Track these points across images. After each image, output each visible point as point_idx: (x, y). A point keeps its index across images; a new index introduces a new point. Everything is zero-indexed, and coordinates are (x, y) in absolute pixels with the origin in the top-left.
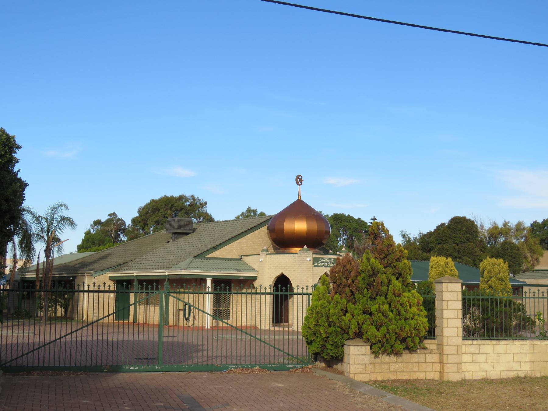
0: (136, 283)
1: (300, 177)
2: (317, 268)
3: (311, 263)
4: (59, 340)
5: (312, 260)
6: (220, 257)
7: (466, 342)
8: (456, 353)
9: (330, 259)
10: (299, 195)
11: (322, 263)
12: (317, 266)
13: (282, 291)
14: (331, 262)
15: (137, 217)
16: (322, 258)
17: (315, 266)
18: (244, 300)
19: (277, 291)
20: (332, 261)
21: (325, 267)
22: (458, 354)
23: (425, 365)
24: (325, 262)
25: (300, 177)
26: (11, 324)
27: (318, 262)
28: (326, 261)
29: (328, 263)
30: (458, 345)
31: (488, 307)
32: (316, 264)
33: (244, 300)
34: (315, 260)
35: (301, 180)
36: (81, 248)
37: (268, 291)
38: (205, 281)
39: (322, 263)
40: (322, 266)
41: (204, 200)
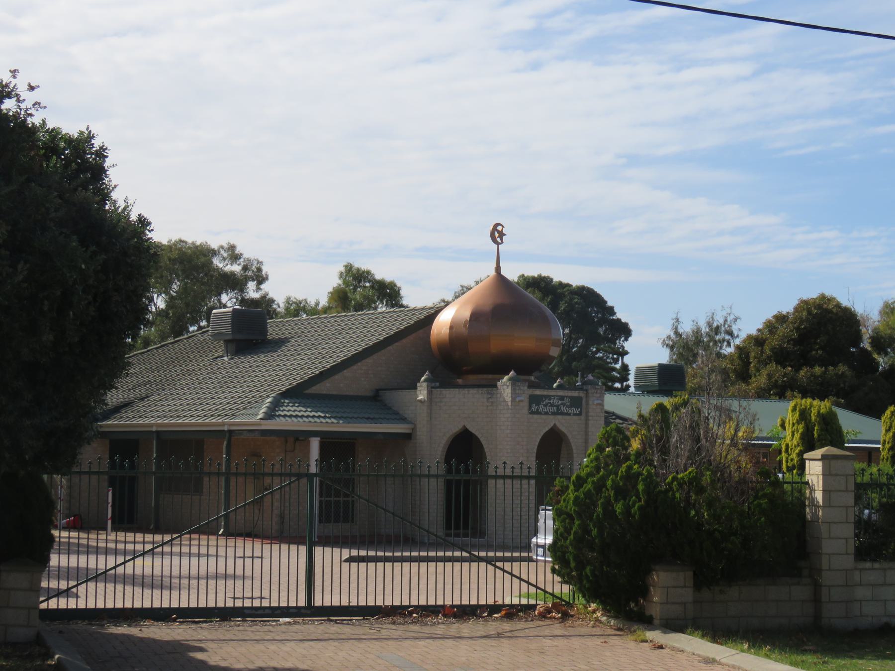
0: (656, 622)
1: (499, 228)
2: (535, 416)
3: (526, 404)
4: (113, 572)
5: (527, 400)
6: (334, 393)
7: (862, 565)
9: (562, 398)
10: (498, 269)
12: (538, 413)
13: (458, 471)
14: (564, 405)
17: (532, 413)
18: (275, 554)
19: (449, 471)
20: (567, 402)
21: (553, 414)
22: (847, 586)
24: (552, 405)
25: (499, 228)
26: (142, 539)
27: (538, 404)
28: (555, 401)
29: (558, 406)
30: (847, 570)
32: (534, 408)
33: (275, 554)
34: (534, 400)
35: (502, 235)
37: (433, 471)
39: (545, 406)
40: (546, 413)
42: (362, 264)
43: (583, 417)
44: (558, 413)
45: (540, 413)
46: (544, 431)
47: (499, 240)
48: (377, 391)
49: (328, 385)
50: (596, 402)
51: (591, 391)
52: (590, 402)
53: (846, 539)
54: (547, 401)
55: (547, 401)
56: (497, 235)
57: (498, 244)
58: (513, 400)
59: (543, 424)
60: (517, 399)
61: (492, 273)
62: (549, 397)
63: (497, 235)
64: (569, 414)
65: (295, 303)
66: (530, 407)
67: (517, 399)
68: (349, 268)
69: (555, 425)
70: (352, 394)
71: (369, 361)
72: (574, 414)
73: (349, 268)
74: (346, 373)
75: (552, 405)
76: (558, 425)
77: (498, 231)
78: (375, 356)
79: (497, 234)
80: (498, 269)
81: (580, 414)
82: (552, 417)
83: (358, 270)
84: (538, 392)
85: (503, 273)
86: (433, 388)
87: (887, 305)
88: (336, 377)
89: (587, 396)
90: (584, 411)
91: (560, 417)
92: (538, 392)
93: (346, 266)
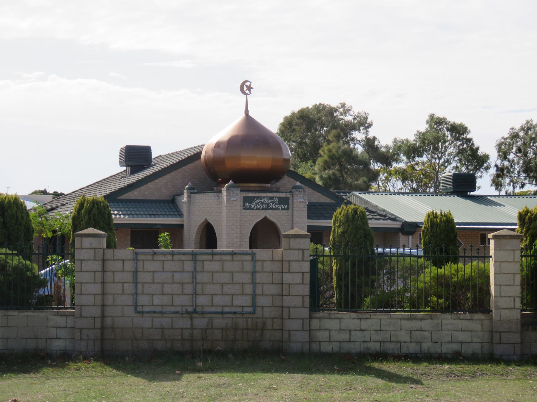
2: (248, 211)
6: (141, 198)
8: (214, 274)
10: (247, 111)
11: (257, 204)
12: (250, 208)
14: (273, 203)
15: (287, 175)
16: (258, 198)
17: (246, 209)
20: (276, 200)
21: (264, 209)
23: (112, 262)
24: (263, 203)
28: (266, 201)
29: (268, 204)
31: (348, 273)
32: (247, 205)
34: (246, 200)
35: (249, 88)
36: (106, 197)
38: (484, 240)
39: (257, 204)
40: (258, 209)
41: (524, 122)
42: (439, 114)
43: (290, 211)
44: (268, 208)
45: (253, 209)
46: (257, 221)
47: (247, 92)
48: (174, 196)
49: (135, 193)
50: (299, 200)
51: (296, 193)
52: (295, 201)
53: (303, 296)
54: (258, 200)
55: (258, 200)
56: (245, 88)
57: (247, 94)
58: (228, 200)
59: (255, 217)
60: (231, 199)
61: (243, 115)
62: (260, 198)
63: (245, 88)
64: (279, 209)
65: (400, 142)
66: (244, 205)
67: (231, 199)
68: (432, 117)
69: (266, 216)
70: (154, 199)
71: (168, 176)
72: (282, 209)
73: (432, 117)
74: (150, 185)
75: (263, 203)
76: (268, 217)
77: (246, 86)
78: (173, 173)
79: (246, 88)
80: (247, 111)
81: (288, 209)
82: (263, 211)
83: (438, 118)
84: (251, 194)
85: (250, 114)
86: (191, 193)
87: (528, 128)
88: (142, 188)
89: (293, 197)
90: (290, 206)
91: (270, 211)
92: (251, 194)
93: (430, 116)
